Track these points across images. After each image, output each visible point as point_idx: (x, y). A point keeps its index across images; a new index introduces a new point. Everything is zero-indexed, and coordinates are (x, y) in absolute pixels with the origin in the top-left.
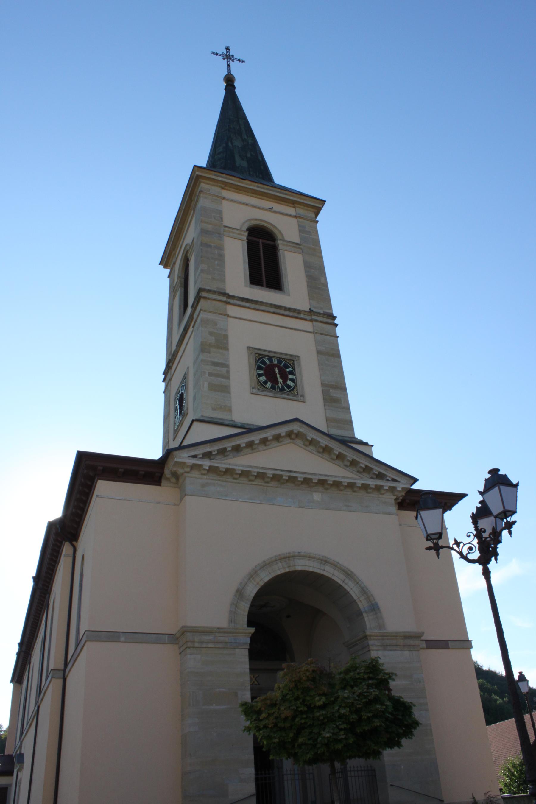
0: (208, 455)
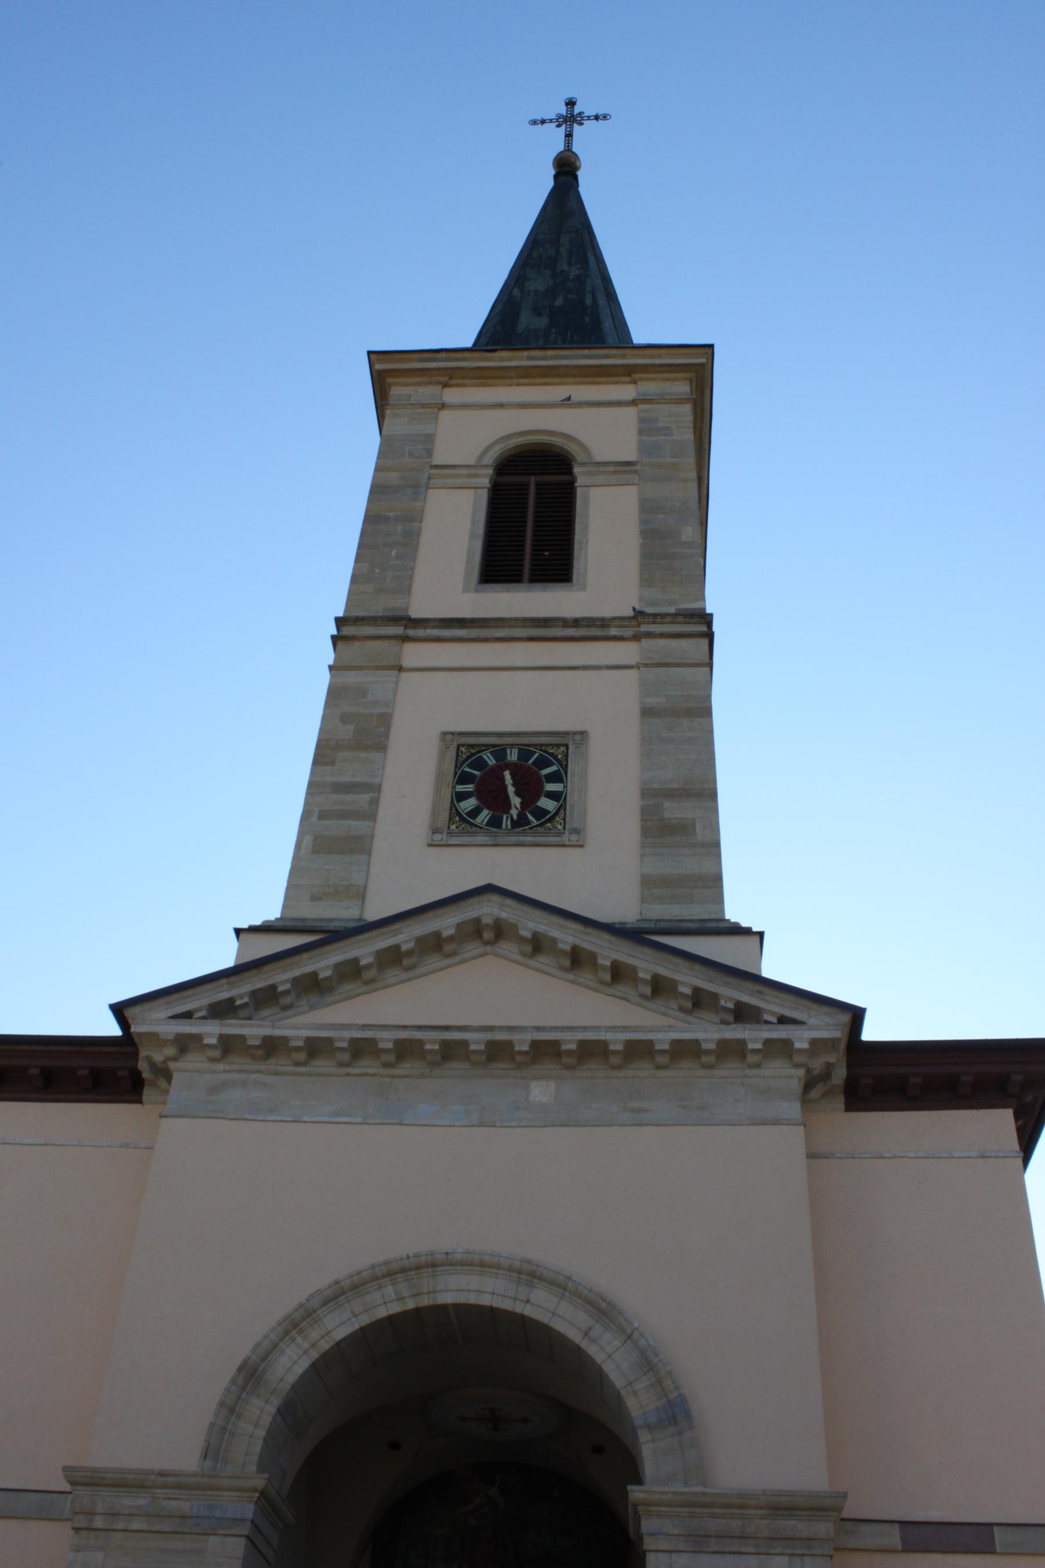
0: (221, 1010)
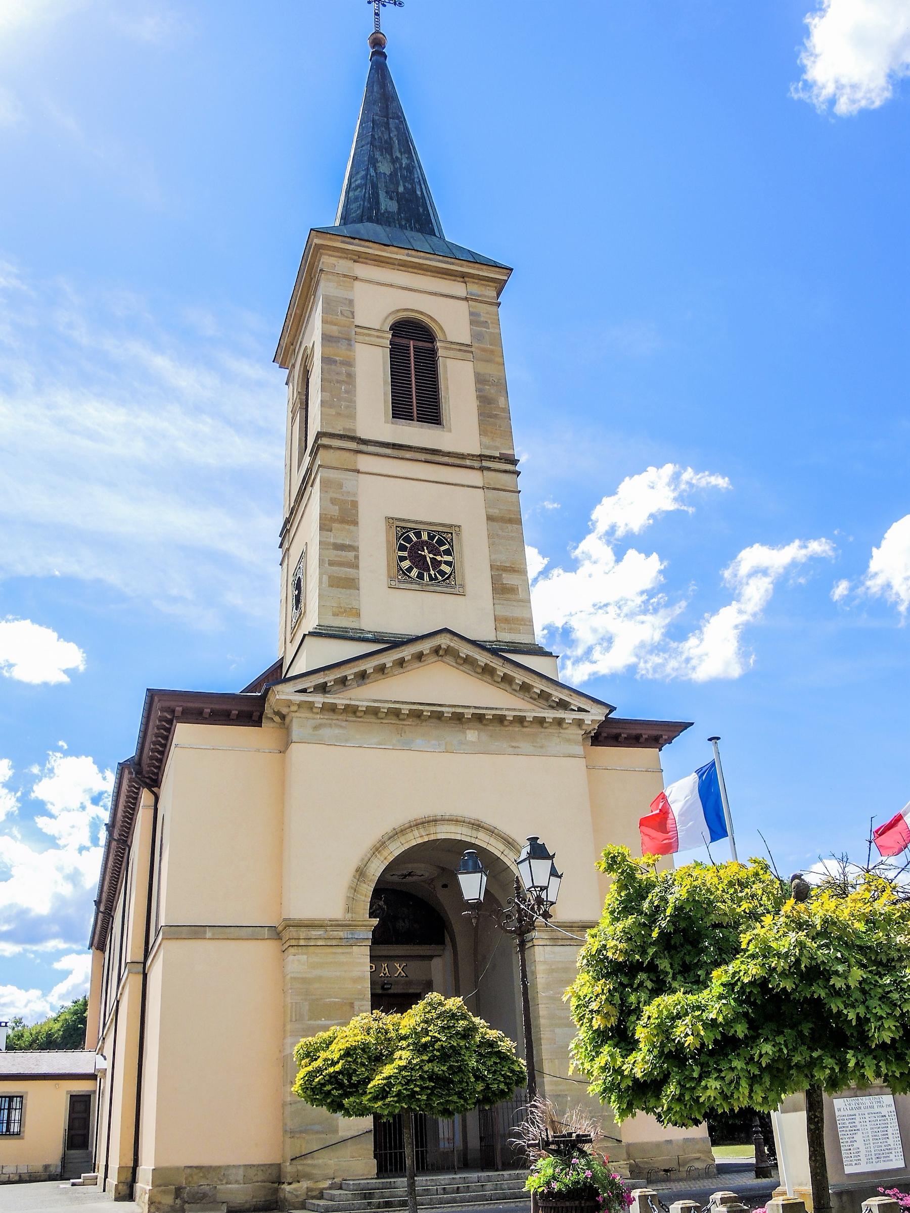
0: (323, 688)
